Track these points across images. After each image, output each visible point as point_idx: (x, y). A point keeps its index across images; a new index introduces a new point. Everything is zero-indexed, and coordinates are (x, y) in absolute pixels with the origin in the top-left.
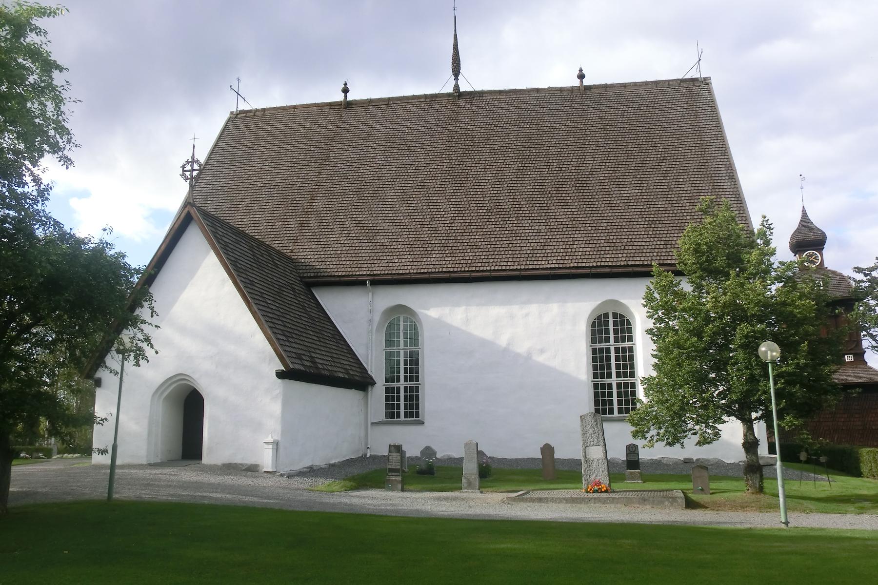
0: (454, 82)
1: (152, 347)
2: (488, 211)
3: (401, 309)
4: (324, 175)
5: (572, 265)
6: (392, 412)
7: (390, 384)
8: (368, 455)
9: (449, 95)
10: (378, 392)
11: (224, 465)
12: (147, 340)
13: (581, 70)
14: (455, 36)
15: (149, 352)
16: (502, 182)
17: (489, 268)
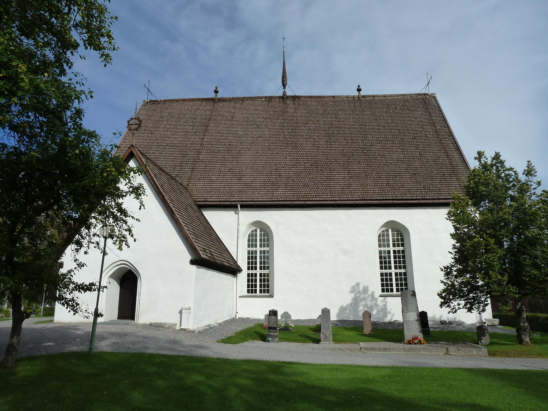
0: (286, 90)
1: (132, 236)
2: (311, 165)
3: (258, 224)
4: (205, 140)
5: (368, 198)
6: (251, 289)
7: (251, 272)
8: (237, 318)
9: (280, 97)
10: (243, 277)
11: (151, 324)
12: (130, 230)
13: (359, 86)
14: (284, 63)
15: (130, 240)
16: (318, 148)
17: (316, 199)
